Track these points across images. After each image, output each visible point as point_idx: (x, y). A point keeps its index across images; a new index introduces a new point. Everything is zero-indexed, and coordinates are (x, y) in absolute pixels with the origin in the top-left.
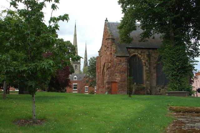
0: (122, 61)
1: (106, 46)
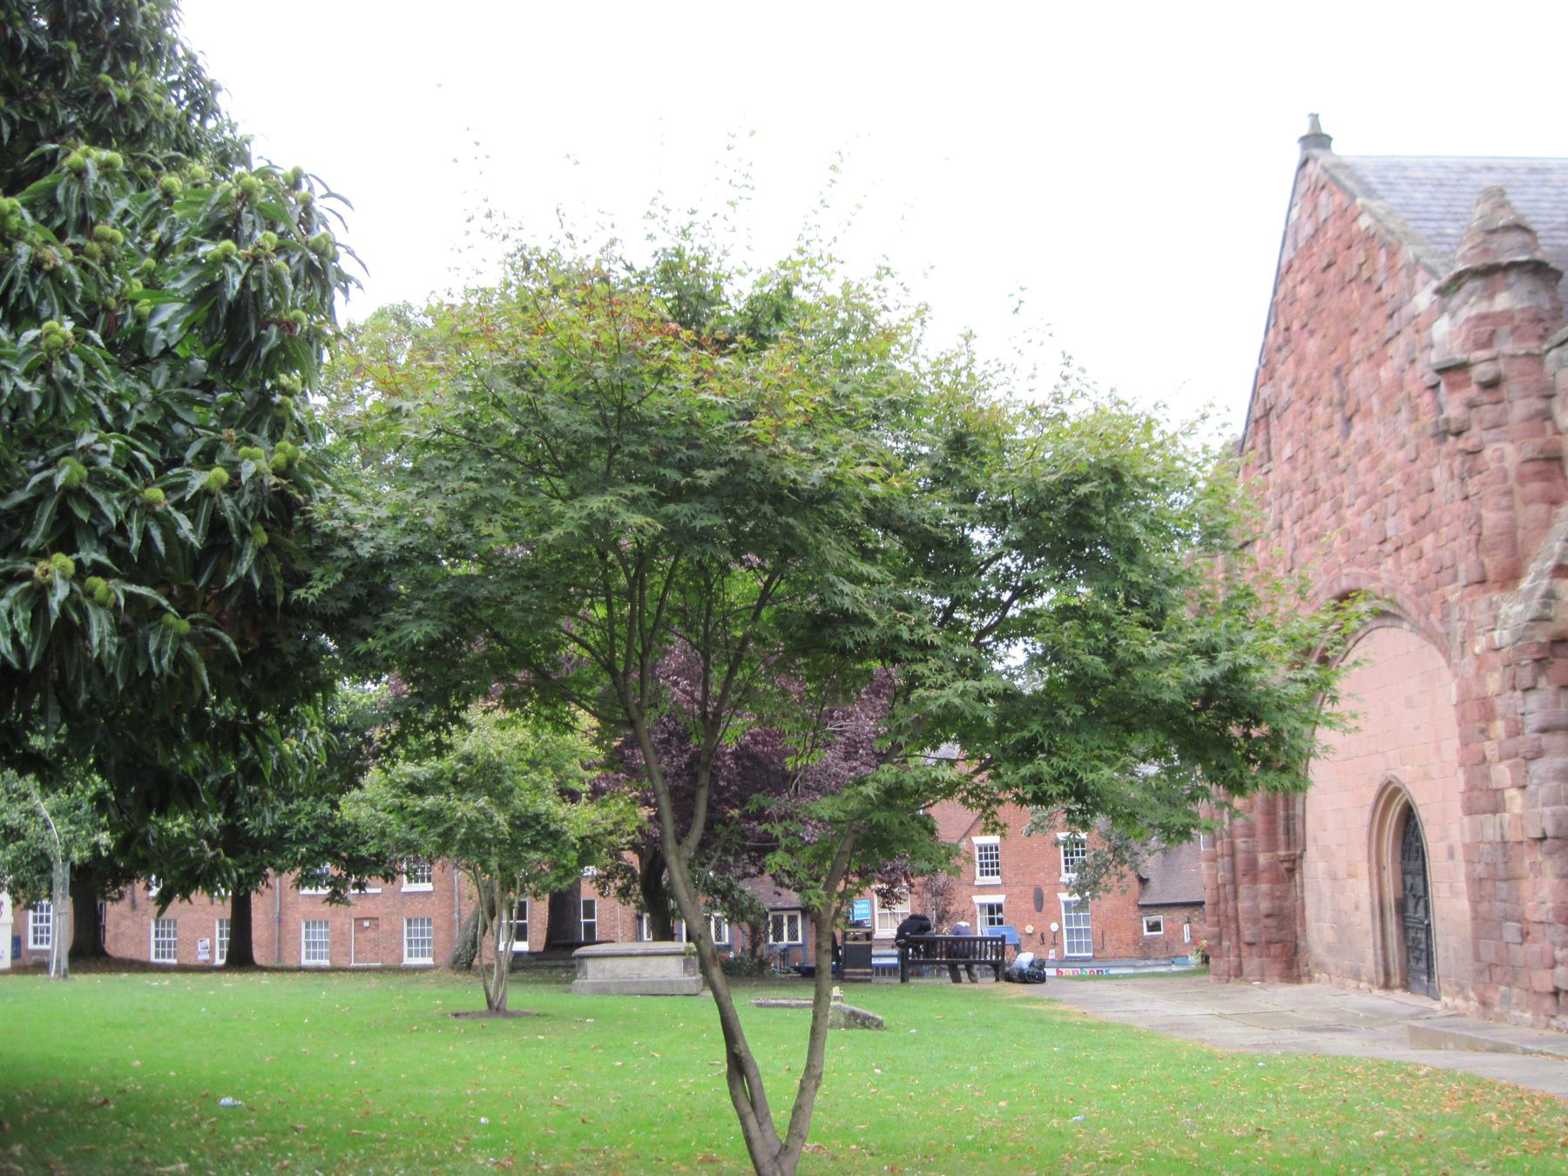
1: (1463, 367)
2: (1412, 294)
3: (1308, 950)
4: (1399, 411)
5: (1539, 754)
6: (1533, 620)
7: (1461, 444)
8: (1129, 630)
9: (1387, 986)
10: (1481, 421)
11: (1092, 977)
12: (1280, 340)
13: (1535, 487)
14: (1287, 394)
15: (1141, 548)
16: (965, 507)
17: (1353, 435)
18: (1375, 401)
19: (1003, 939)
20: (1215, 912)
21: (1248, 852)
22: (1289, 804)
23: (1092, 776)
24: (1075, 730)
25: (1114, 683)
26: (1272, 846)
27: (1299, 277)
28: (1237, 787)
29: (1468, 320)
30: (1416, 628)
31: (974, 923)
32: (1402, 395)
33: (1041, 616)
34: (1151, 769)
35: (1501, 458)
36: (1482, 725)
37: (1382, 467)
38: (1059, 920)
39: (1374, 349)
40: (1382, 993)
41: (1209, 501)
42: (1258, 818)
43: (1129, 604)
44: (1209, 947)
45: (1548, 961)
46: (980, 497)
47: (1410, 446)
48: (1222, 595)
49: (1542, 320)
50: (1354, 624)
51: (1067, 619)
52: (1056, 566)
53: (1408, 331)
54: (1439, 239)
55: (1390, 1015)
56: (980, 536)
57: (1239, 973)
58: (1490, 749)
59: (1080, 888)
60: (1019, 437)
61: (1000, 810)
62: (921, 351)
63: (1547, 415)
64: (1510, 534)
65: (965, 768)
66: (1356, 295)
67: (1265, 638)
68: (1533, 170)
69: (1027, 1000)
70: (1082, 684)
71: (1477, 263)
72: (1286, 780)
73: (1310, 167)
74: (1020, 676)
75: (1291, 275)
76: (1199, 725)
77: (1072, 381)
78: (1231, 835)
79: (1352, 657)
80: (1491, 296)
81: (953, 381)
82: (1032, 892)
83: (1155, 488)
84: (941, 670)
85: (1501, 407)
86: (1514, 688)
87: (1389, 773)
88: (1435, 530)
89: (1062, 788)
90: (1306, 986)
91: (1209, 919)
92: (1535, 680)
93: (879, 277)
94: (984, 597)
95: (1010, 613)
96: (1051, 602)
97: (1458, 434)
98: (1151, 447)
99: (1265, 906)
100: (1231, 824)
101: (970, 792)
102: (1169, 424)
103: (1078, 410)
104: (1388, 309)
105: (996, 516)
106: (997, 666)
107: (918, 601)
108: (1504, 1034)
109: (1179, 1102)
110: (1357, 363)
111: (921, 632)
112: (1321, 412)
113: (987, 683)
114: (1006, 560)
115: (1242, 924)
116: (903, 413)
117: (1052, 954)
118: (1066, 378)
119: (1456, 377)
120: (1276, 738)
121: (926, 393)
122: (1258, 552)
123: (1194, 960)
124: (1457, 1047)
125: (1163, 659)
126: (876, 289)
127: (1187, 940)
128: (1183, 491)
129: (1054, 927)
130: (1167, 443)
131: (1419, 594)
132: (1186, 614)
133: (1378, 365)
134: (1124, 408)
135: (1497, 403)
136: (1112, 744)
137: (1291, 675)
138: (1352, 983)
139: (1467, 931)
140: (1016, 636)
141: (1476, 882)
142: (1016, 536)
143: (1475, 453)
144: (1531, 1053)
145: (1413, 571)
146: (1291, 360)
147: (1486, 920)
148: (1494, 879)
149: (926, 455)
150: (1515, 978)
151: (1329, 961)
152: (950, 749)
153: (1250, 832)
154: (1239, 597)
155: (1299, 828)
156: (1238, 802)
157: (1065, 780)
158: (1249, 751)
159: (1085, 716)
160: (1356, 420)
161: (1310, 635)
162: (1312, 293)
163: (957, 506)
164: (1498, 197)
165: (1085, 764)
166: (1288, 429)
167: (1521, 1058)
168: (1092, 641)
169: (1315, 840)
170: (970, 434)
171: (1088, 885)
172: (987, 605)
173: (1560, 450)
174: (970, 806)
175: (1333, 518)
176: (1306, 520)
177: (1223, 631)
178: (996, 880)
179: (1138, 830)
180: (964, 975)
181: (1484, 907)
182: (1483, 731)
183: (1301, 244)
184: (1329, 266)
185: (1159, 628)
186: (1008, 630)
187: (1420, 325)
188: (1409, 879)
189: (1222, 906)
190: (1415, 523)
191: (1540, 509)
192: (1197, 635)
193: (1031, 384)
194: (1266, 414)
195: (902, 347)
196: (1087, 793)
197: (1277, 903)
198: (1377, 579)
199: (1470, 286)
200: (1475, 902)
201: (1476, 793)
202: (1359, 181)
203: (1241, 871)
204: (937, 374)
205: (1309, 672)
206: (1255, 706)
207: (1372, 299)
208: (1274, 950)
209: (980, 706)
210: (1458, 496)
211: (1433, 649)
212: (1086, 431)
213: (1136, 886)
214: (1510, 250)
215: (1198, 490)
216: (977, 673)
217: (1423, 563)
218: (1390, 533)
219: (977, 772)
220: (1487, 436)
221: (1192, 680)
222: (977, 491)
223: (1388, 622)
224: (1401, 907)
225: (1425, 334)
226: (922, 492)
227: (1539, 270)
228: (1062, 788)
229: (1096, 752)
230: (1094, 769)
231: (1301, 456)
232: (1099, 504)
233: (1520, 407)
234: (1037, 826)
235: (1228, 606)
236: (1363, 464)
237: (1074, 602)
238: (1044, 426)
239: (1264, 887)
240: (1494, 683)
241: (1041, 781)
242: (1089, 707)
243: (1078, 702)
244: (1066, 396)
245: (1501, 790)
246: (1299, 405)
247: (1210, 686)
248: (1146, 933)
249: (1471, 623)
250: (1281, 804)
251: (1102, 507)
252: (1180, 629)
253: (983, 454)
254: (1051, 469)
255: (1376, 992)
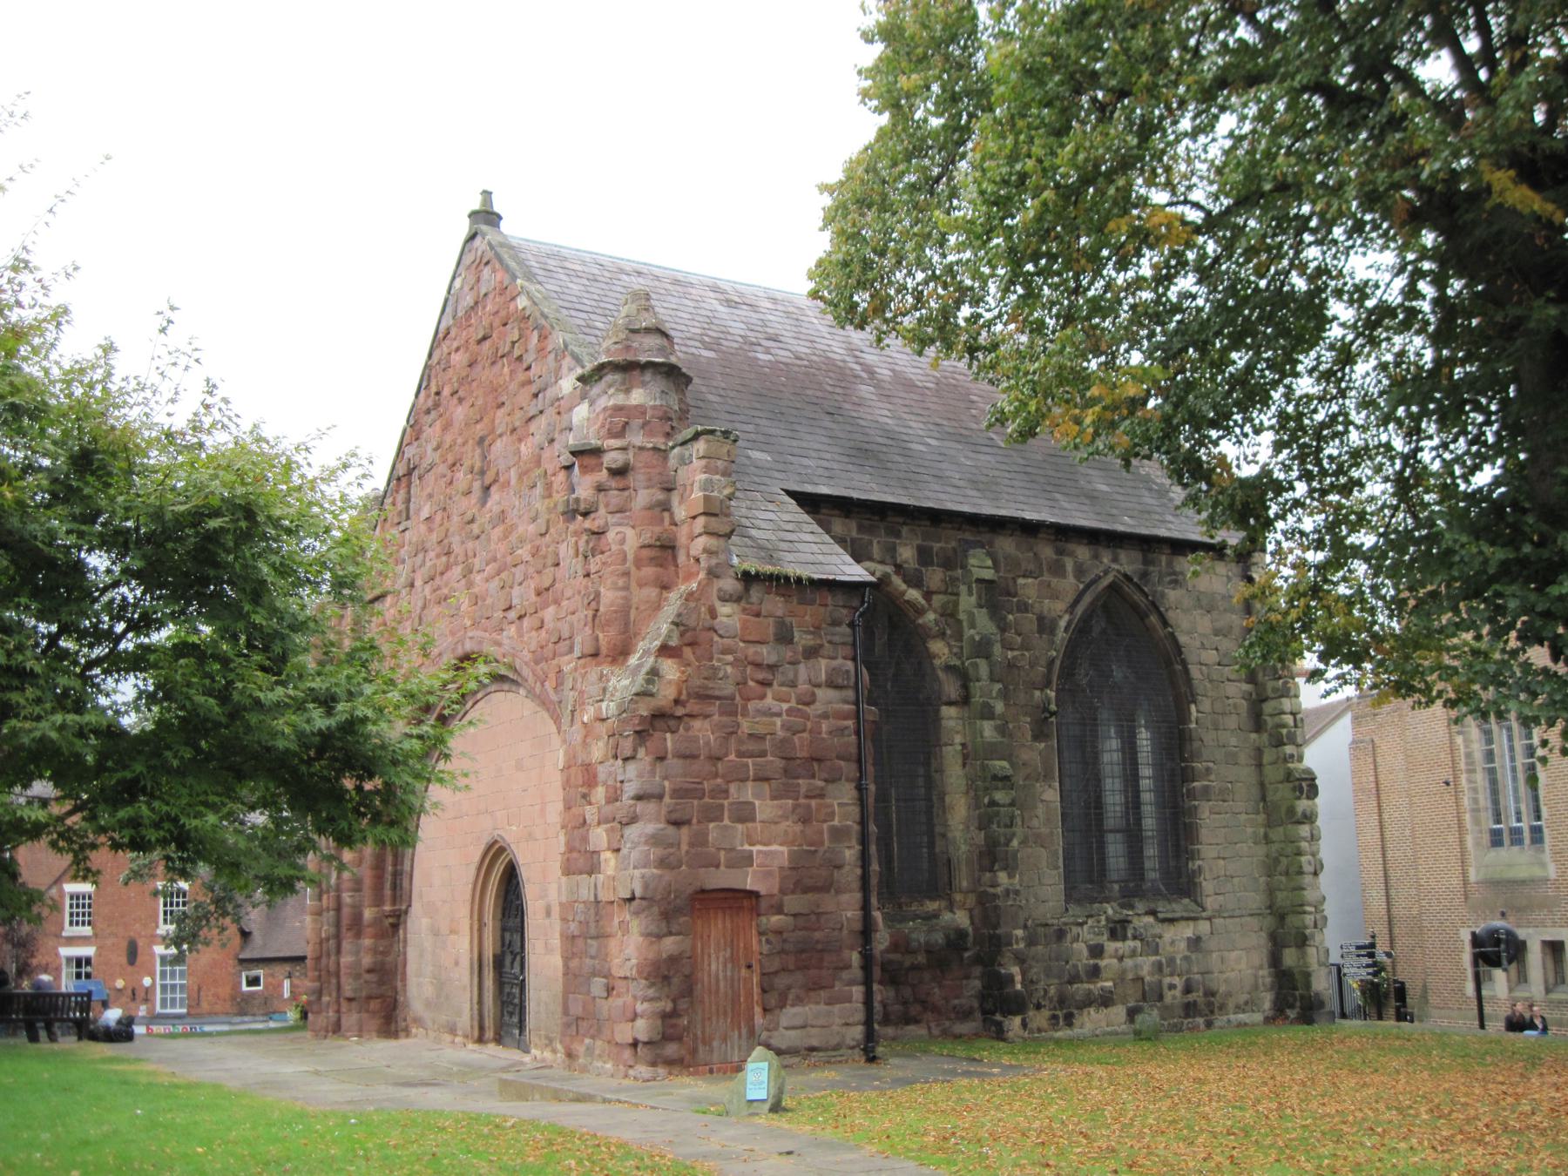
0: (802, 639)
1: (597, 452)
2: (558, 378)
3: (407, 1005)
4: (534, 486)
5: (633, 819)
6: (637, 694)
7: (588, 524)
8: (247, 673)
9: (480, 1040)
10: (607, 505)
11: (185, 1035)
12: (430, 403)
13: (649, 571)
14: (431, 456)
15: (269, 590)
16: (84, 528)
17: (489, 504)
18: (513, 473)
19: (89, 994)
20: (317, 968)
21: (353, 906)
22: (398, 860)
23: (195, 822)
24: (181, 773)
25: (226, 727)
26: (378, 901)
27: (455, 345)
28: (344, 840)
29: (605, 409)
30: (531, 693)
31: (58, 978)
32: (538, 472)
33: (155, 651)
34: (259, 818)
35: (623, 541)
36: (584, 790)
37: (513, 538)
38: (152, 975)
39: (517, 424)
40: (476, 1047)
41: (343, 551)
42: (366, 873)
43: (249, 645)
44: (309, 1003)
45: (629, 1015)
46: (101, 519)
47: (541, 521)
48: (347, 644)
49: (670, 419)
50: (473, 685)
51: (183, 656)
52: (177, 601)
53: (551, 411)
54: (587, 330)
55: (482, 1068)
56: (98, 561)
57: (337, 1029)
58: (591, 813)
59: (177, 941)
60: (152, 462)
61: (93, 855)
62: (54, 356)
63: (665, 507)
64: (624, 611)
65: (56, 810)
66: (506, 370)
67: (384, 692)
68: (676, 282)
69: (112, 1060)
70: (193, 726)
71: (618, 358)
72: (394, 834)
73: (478, 241)
74: (127, 712)
75: (447, 342)
76: (312, 775)
77: (215, 411)
78: (338, 889)
79: (468, 717)
80: (628, 391)
81: (85, 393)
82: (124, 944)
83: (289, 532)
84: (38, 701)
85: (626, 493)
86: (616, 757)
87: (496, 833)
88: (557, 602)
89: (162, 833)
90: (403, 1041)
91: (310, 974)
92: (635, 750)
93: (15, 269)
94: (95, 626)
95: (122, 646)
96: (169, 638)
97: (585, 514)
98: (289, 489)
99: (367, 961)
100: (339, 877)
101: (61, 835)
102: (312, 466)
103: (218, 440)
104: (534, 388)
105: (115, 541)
106: (103, 701)
107: (20, 624)
108: (586, 1084)
109: (267, 1164)
110: (501, 436)
111: (20, 658)
112: (462, 477)
113: (90, 718)
114: (124, 590)
115: (343, 979)
116: (26, 421)
117: (142, 1011)
118: (207, 407)
119: (588, 461)
120: (388, 793)
121: (53, 402)
122: (387, 607)
123: (292, 1015)
124: (543, 1098)
125: (279, 707)
126: (10, 281)
127: (286, 995)
128: (317, 537)
129: (147, 981)
130: (306, 488)
131: (537, 662)
132: (309, 661)
133: (520, 440)
134: (264, 445)
135: (623, 490)
136: (220, 789)
137: (407, 730)
138: (448, 1037)
139: (558, 987)
140: (127, 671)
141: (569, 939)
142: (137, 565)
143: (599, 534)
144: (610, 1101)
145: (533, 639)
146: (438, 424)
147: (575, 976)
148: (585, 936)
149: (47, 469)
150: (599, 1031)
151: (427, 1016)
152: (42, 788)
153: (357, 886)
154: (364, 649)
155: (405, 884)
156: (347, 855)
157: (166, 825)
158: (359, 804)
159: (193, 760)
160: (493, 489)
161: (430, 693)
162: (465, 362)
163: (75, 526)
164: (644, 300)
165: (189, 810)
166: (429, 490)
167: (601, 1107)
168: (207, 682)
169: (421, 897)
170: (96, 451)
171: (188, 935)
172: (98, 635)
173: (674, 539)
174: (60, 850)
175: (463, 582)
176: (438, 581)
177: (343, 681)
178: (87, 930)
179: (242, 882)
180: (43, 1034)
181: (574, 963)
182: (584, 796)
183: (460, 314)
184: (484, 338)
185: (279, 674)
186: (119, 664)
187: (562, 408)
188: (507, 936)
189: (324, 961)
190: (539, 594)
191: (652, 592)
192: (317, 684)
193: (171, 408)
194: (409, 473)
195: (33, 348)
196: (189, 839)
197: (380, 958)
198: (499, 644)
199: (609, 378)
200: (566, 959)
201: (575, 855)
202: (521, 263)
203: (345, 925)
204: (69, 383)
205: (425, 729)
206: (368, 759)
207: (521, 376)
208: (374, 1005)
209: (79, 743)
210: (581, 572)
211: (546, 715)
212: (221, 463)
213: (237, 939)
214: (647, 347)
215: (332, 538)
216: (79, 707)
217: (543, 632)
218: (515, 602)
219: (70, 813)
220: (611, 519)
221: (308, 728)
222: (99, 513)
223: (506, 687)
224: (499, 963)
225: (565, 416)
226: (37, 506)
227: (673, 374)
228: (162, 833)
229: (202, 798)
230: (198, 815)
231: (438, 518)
232: (229, 541)
233: (643, 497)
234: (136, 874)
235: (351, 657)
236: (498, 531)
237: (194, 639)
238: (179, 453)
239: (367, 942)
240: (598, 750)
241: (139, 825)
242: (198, 750)
243: (186, 744)
244: (206, 426)
245: (598, 853)
246: (442, 469)
247: (325, 736)
248: (245, 988)
249: (582, 692)
250: (389, 859)
251: (231, 544)
252: (301, 676)
253: (110, 474)
254: (182, 499)
255: (471, 1046)
